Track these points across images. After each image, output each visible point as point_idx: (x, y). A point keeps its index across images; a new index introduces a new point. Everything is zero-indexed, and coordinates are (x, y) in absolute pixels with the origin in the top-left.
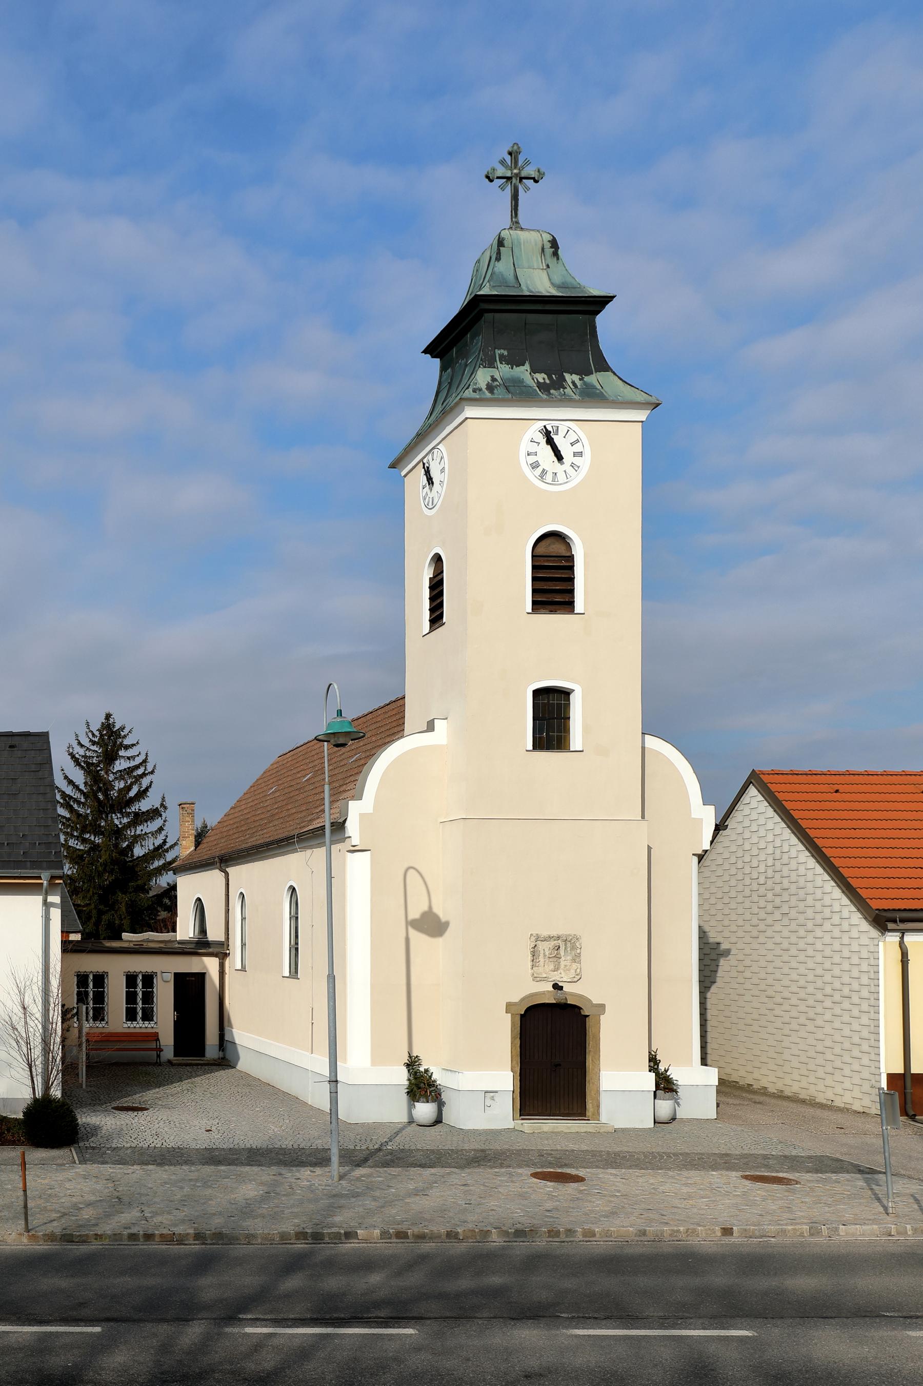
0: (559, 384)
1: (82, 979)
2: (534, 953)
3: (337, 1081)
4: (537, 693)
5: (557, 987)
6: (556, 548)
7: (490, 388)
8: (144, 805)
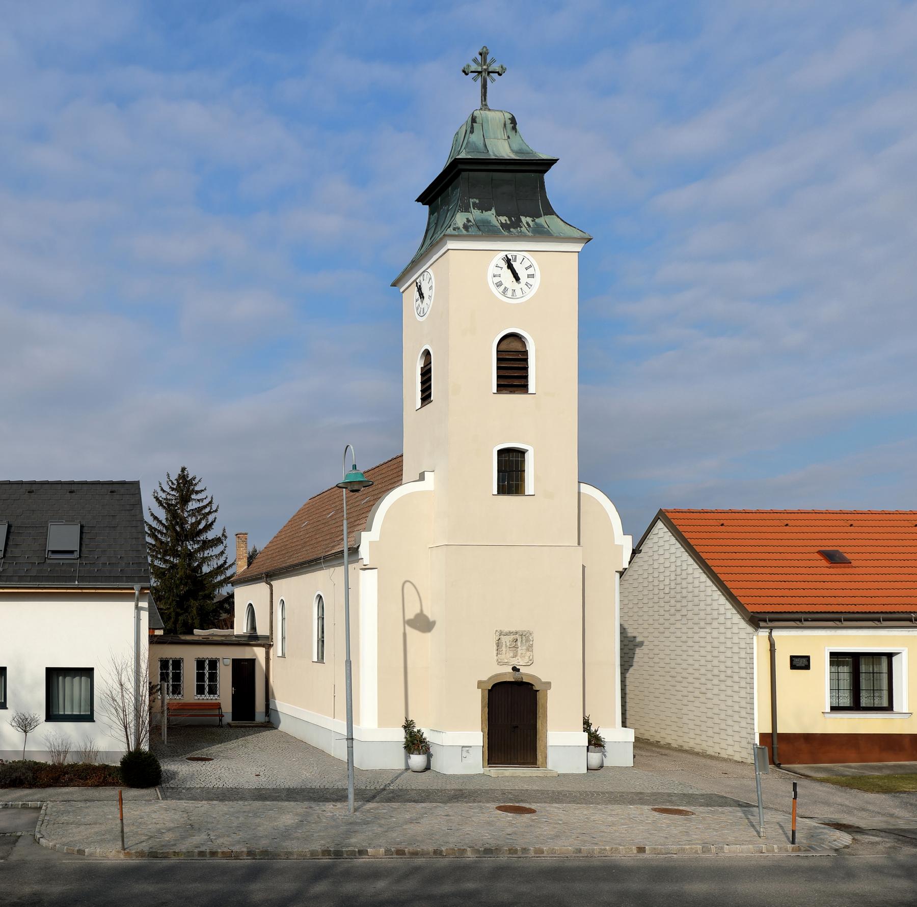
0: (517, 224)
1: (164, 664)
2: (499, 644)
5: (515, 669)
7: (466, 227)
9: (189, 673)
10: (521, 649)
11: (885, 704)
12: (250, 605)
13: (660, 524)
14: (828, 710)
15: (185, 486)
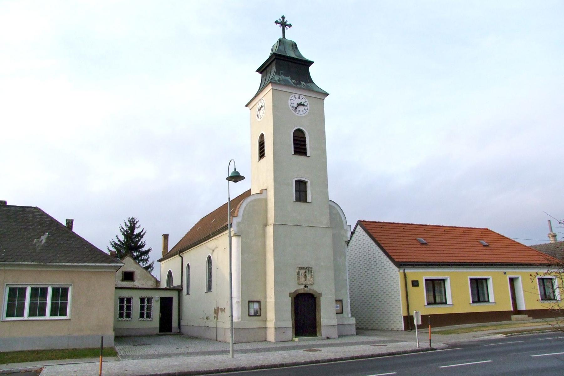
0: (300, 84)
1: (122, 300)
2: (298, 274)
3: (266, 328)
4: (296, 181)
5: (306, 286)
6: (299, 134)
7: (279, 80)
8: (145, 249)
9: (136, 305)
10: (309, 277)
11: (444, 302)
12: (170, 271)
13: (359, 227)
14: (426, 304)
15: (149, 250)
